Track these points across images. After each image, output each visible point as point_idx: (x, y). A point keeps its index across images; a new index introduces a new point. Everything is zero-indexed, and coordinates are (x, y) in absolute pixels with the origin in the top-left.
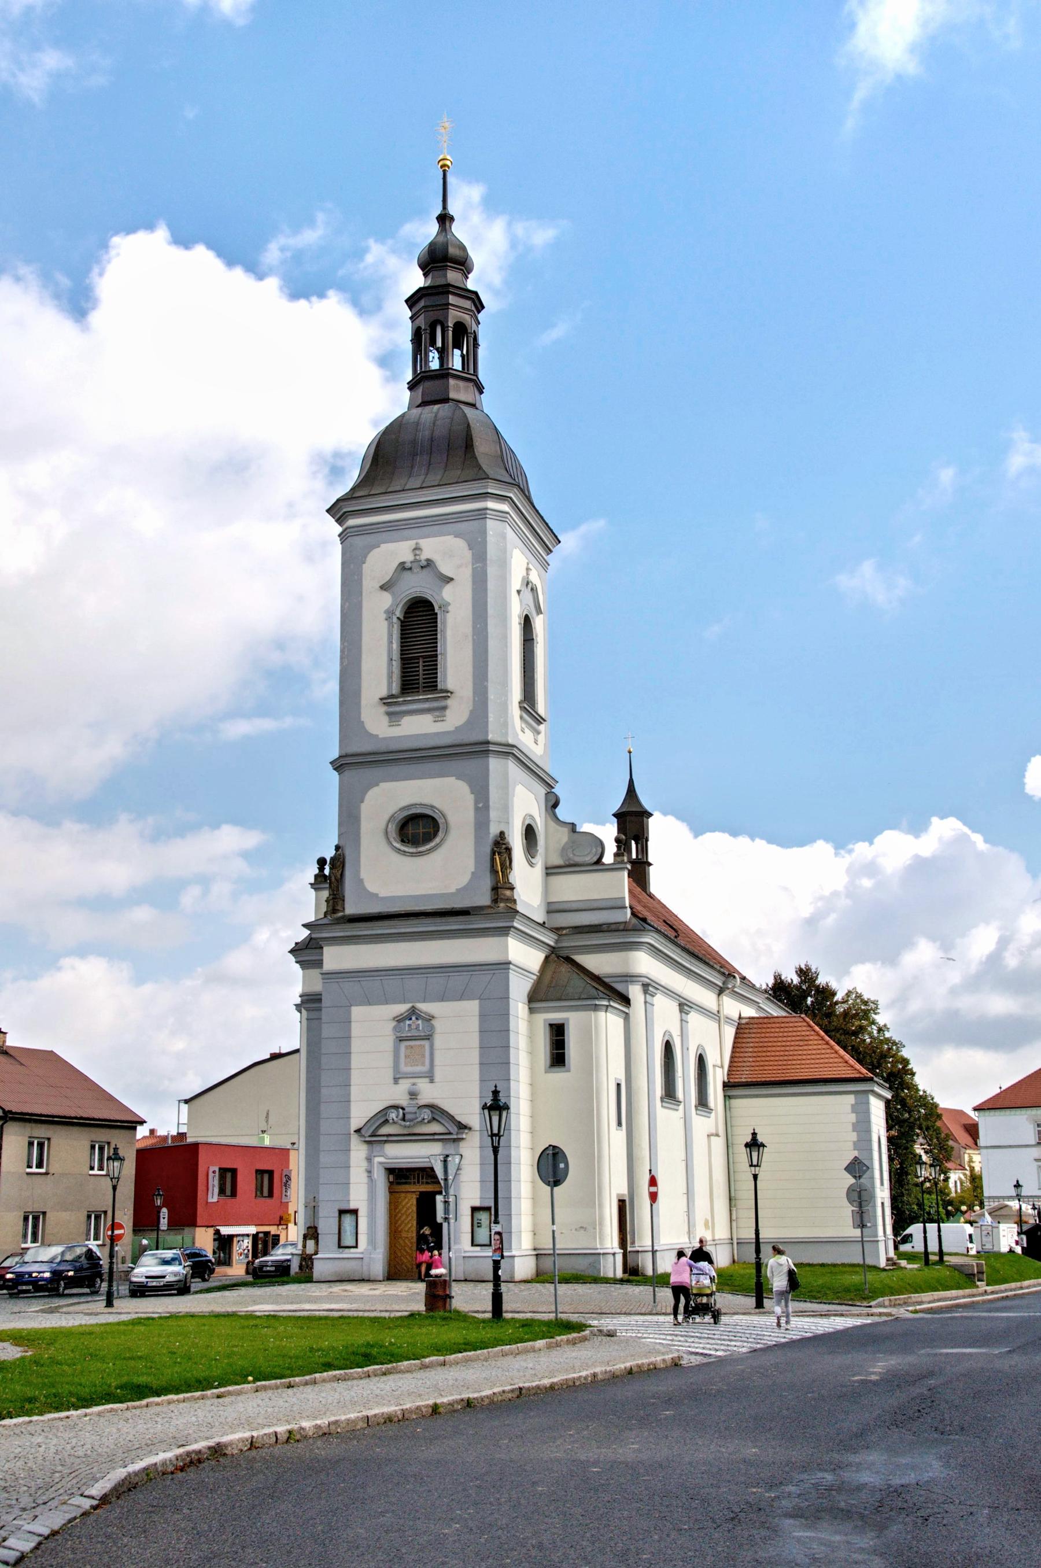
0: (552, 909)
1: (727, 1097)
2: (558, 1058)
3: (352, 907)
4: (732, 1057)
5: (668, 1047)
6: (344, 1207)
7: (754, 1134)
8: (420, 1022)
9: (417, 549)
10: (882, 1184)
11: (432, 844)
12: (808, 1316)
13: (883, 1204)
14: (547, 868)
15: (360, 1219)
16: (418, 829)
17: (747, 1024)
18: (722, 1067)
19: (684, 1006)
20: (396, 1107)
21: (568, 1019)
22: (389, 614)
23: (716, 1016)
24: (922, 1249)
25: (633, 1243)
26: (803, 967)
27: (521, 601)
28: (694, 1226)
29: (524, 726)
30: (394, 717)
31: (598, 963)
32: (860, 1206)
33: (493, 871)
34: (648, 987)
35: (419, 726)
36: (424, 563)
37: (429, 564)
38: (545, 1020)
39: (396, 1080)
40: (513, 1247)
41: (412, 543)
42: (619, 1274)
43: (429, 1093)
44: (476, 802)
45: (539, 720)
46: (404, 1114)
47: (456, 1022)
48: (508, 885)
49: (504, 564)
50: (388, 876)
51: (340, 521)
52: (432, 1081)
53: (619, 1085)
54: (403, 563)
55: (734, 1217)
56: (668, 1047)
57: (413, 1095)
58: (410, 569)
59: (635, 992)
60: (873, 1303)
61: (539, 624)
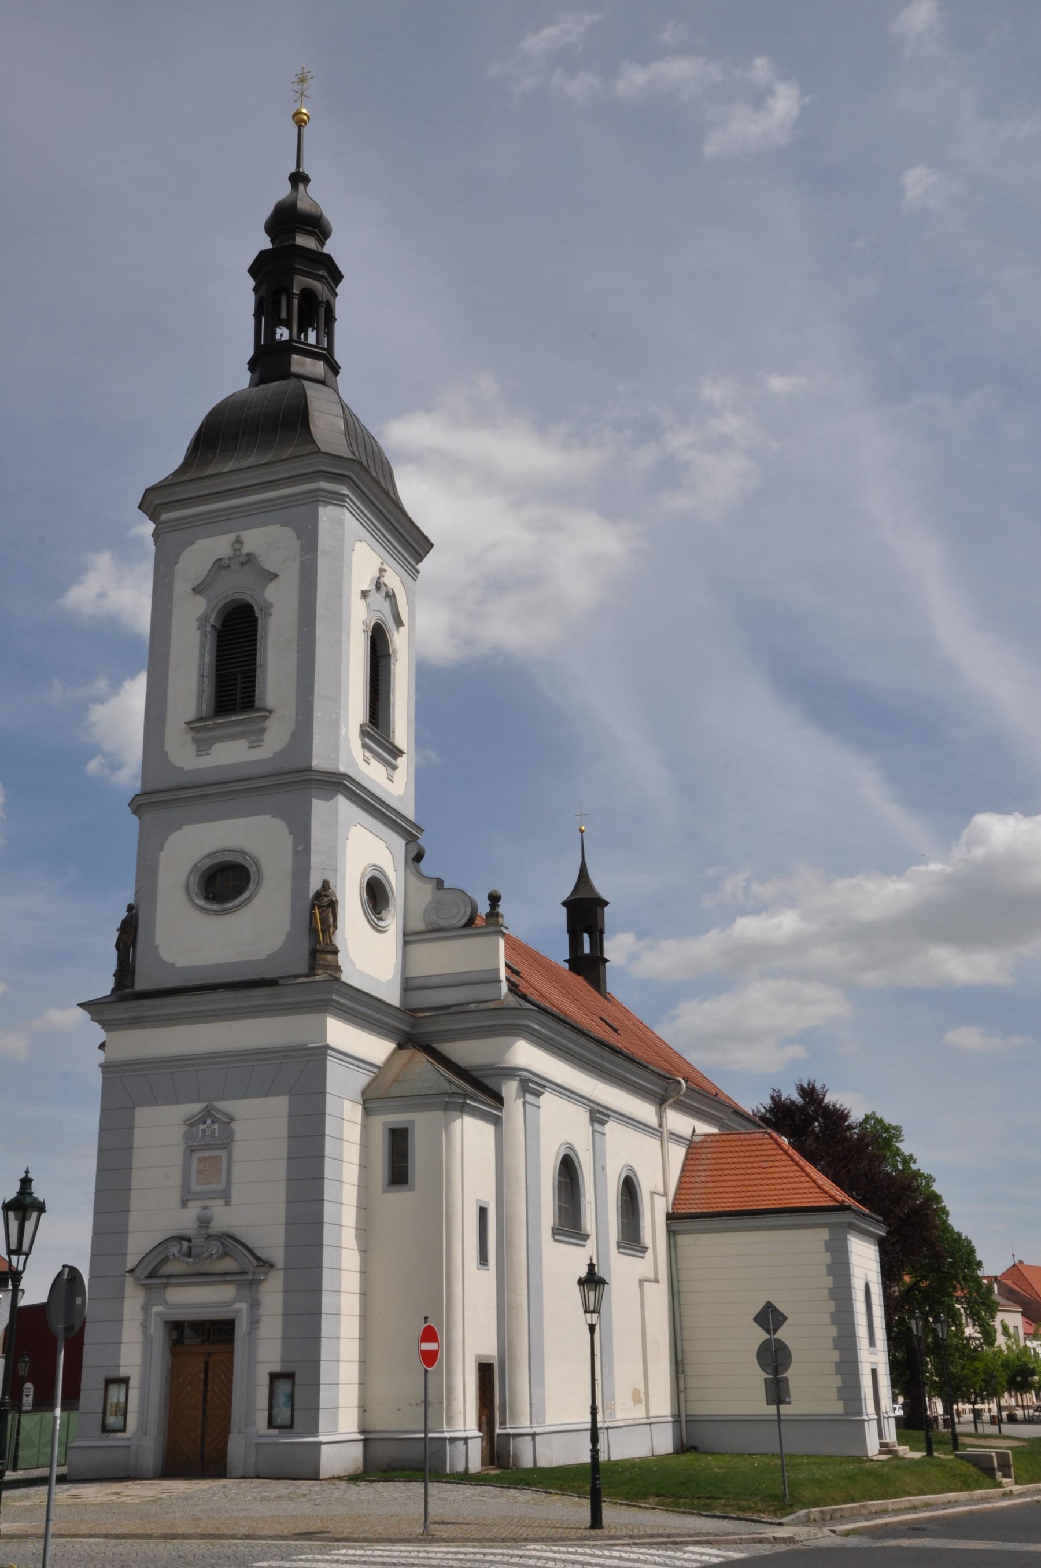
0: (408, 986)
1: (671, 1233)
2: (399, 1174)
3: (141, 984)
4: (680, 1182)
5: (568, 1168)
6: (112, 1374)
7: (26, 1182)
8: (216, 1126)
9: (239, 541)
10: (872, 1342)
11: (237, 902)
12: (651, 1545)
13: (874, 1372)
14: (405, 935)
15: (130, 1392)
16: (225, 882)
17: (702, 1142)
18: (665, 1194)
19: (599, 1115)
20: (180, 1238)
21: (413, 1122)
22: (203, 620)
23: (657, 1132)
24: (587, 1459)
25: (503, 1423)
26: (806, 1086)
27: (368, 605)
28: (613, 1398)
29: (368, 754)
30: (203, 747)
31: (467, 1052)
32: (776, 1372)
33: (313, 931)
34: (533, 1085)
35: (231, 753)
36: (243, 559)
37: (250, 559)
38: (384, 1124)
39: (184, 1204)
40: (322, 1426)
41: (232, 537)
42: (475, 1465)
43: (224, 1218)
44: (295, 844)
45: (397, 753)
46: (190, 1248)
47: (260, 1123)
48: (330, 948)
49: (340, 557)
50: (192, 940)
51: (153, 517)
52: (228, 1203)
53: (483, 1212)
54: (219, 560)
55: (682, 1387)
56: (568, 1168)
57: (204, 1222)
58: (229, 566)
59: (510, 1089)
60: (785, 1520)
61: (399, 641)
